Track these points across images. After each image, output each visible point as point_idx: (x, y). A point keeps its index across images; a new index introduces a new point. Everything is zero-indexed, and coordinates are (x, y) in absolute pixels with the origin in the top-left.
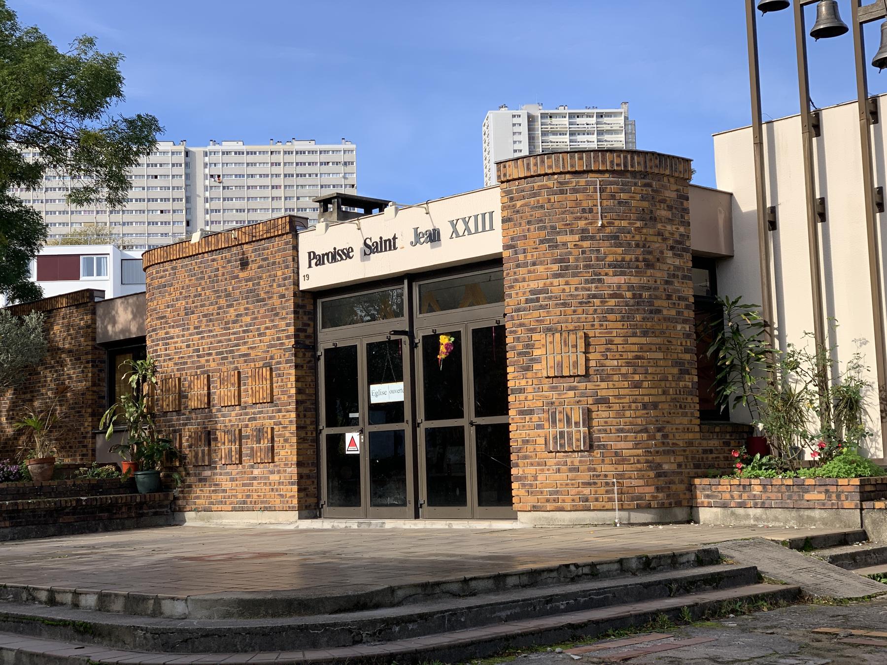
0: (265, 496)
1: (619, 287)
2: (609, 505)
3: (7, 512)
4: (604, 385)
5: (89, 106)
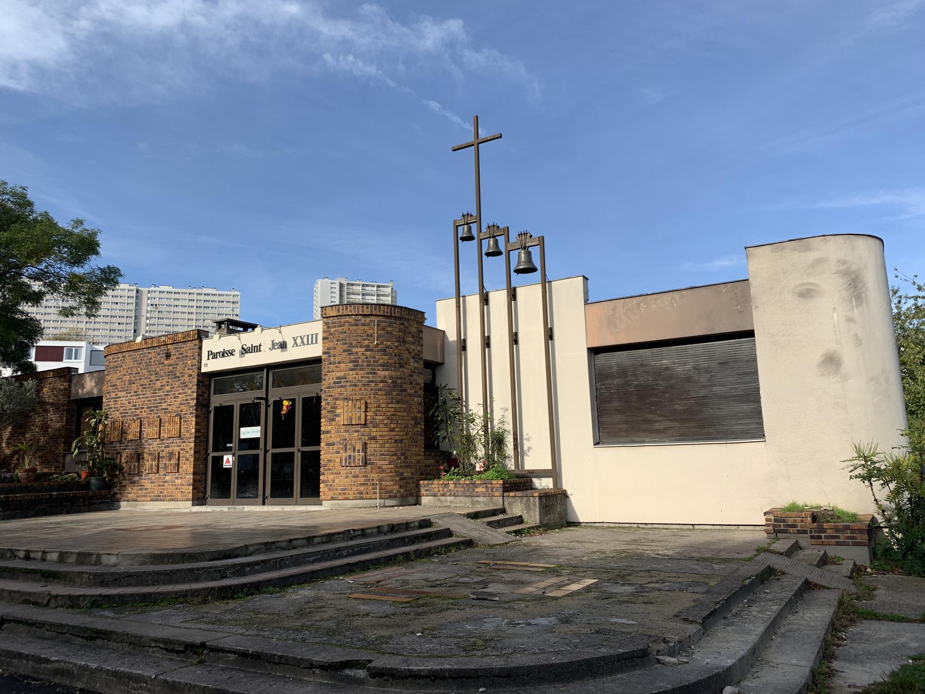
2: (374, 496)
4: (374, 429)
5: (78, 261)
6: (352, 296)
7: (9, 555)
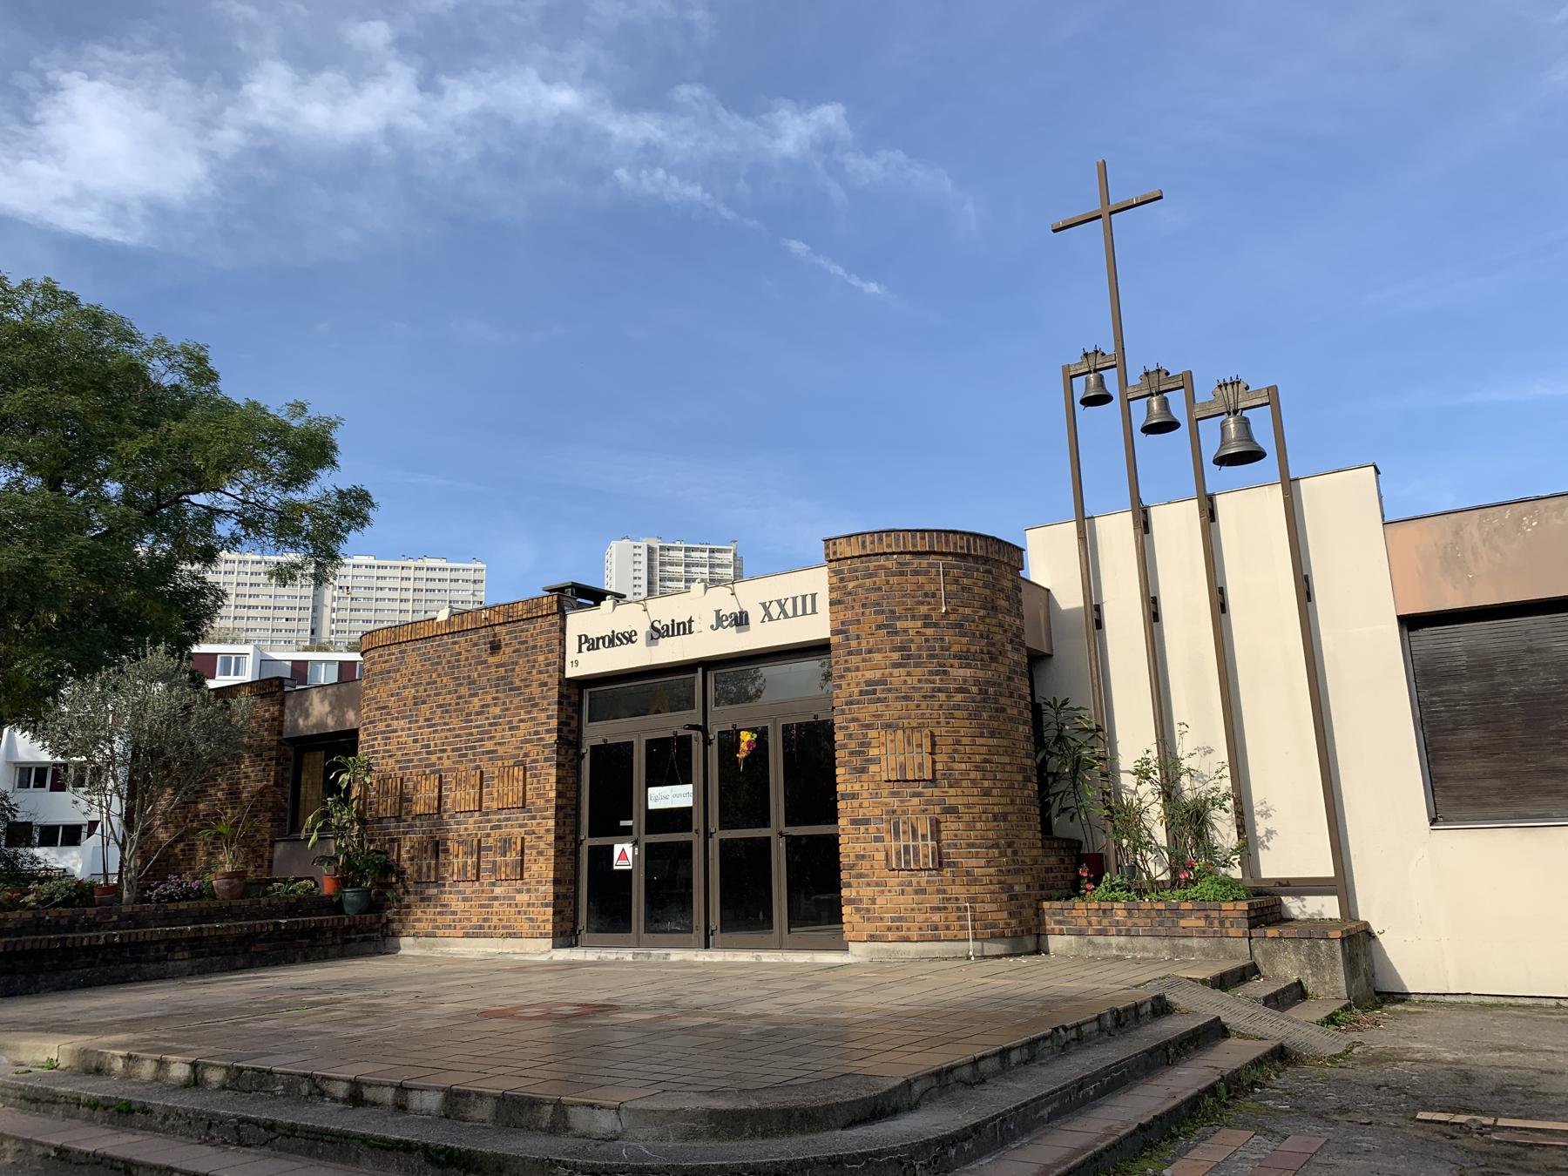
0: (508, 920)
1: (965, 681)
2: (961, 935)
3: (190, 940)
4: (952, 791)
5: (297, 477)
6: (668, 568)
7: (305, 1088)
